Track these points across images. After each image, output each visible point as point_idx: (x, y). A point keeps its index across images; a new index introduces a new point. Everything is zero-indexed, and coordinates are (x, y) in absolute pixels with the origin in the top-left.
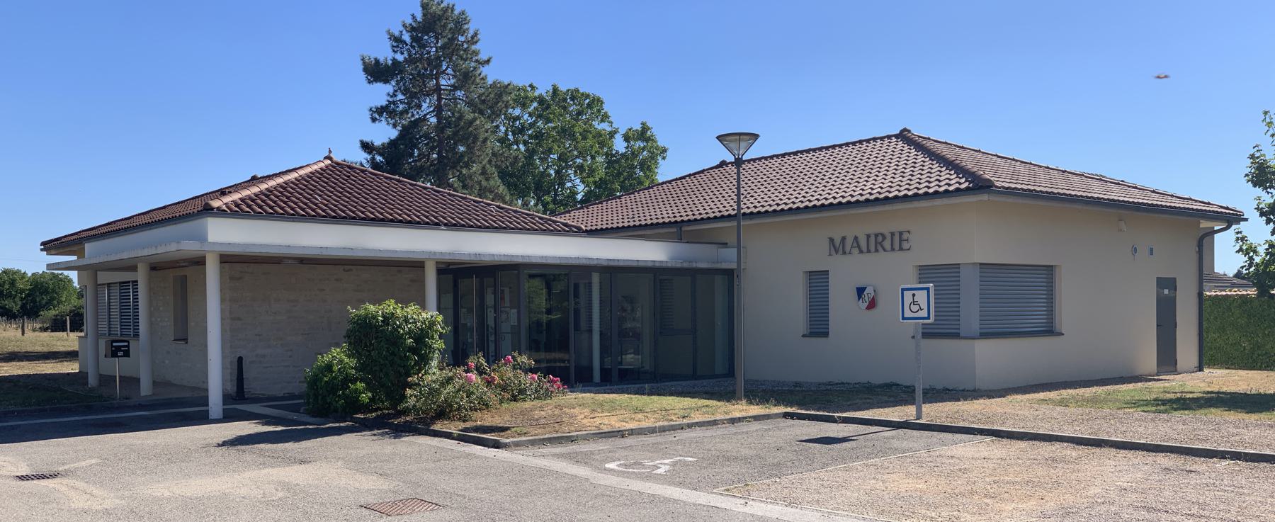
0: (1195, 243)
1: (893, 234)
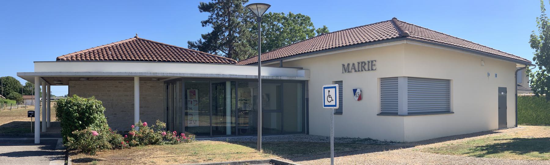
1: (369, 62)
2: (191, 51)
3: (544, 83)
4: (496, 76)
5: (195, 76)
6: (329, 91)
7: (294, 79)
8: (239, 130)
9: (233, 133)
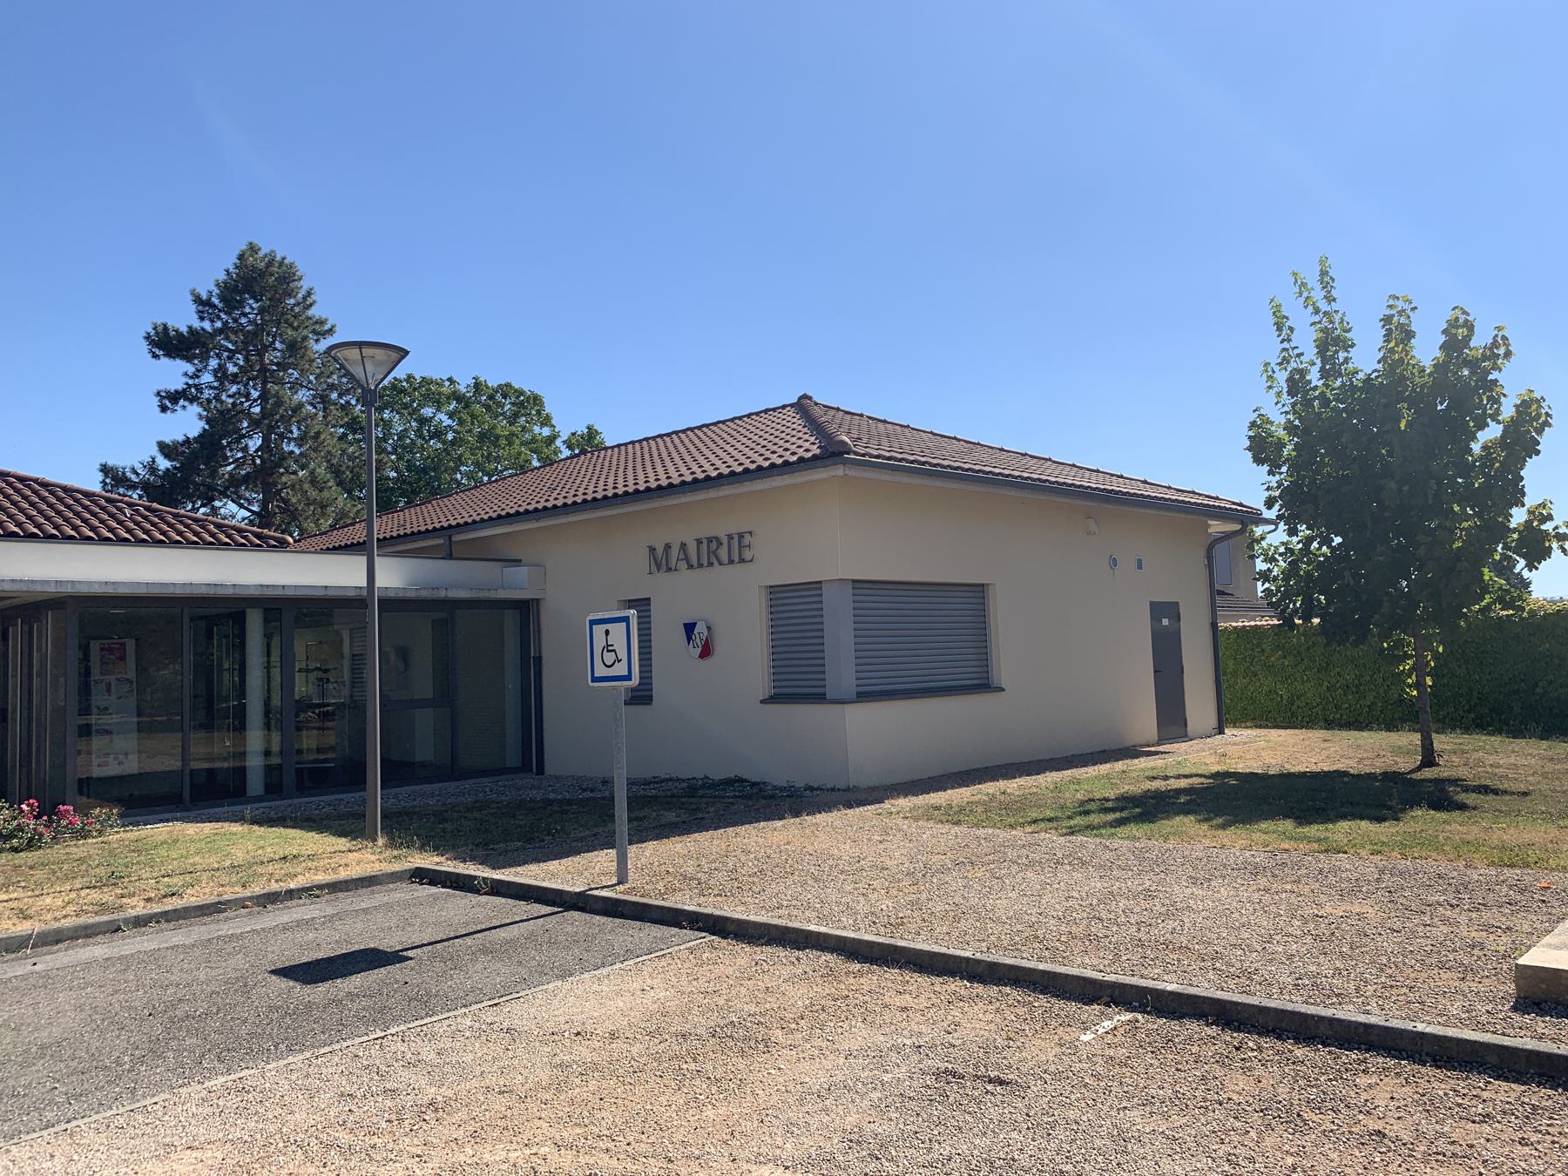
0: (1202, 553)
1: (730, 537)
2: (108, 500)
3: (1302, 580)
4: (1140, 567)
5: (122, 591)
6: (607, 632)
7: (492, 595)
8: (299, 772)
9: (274, 788)
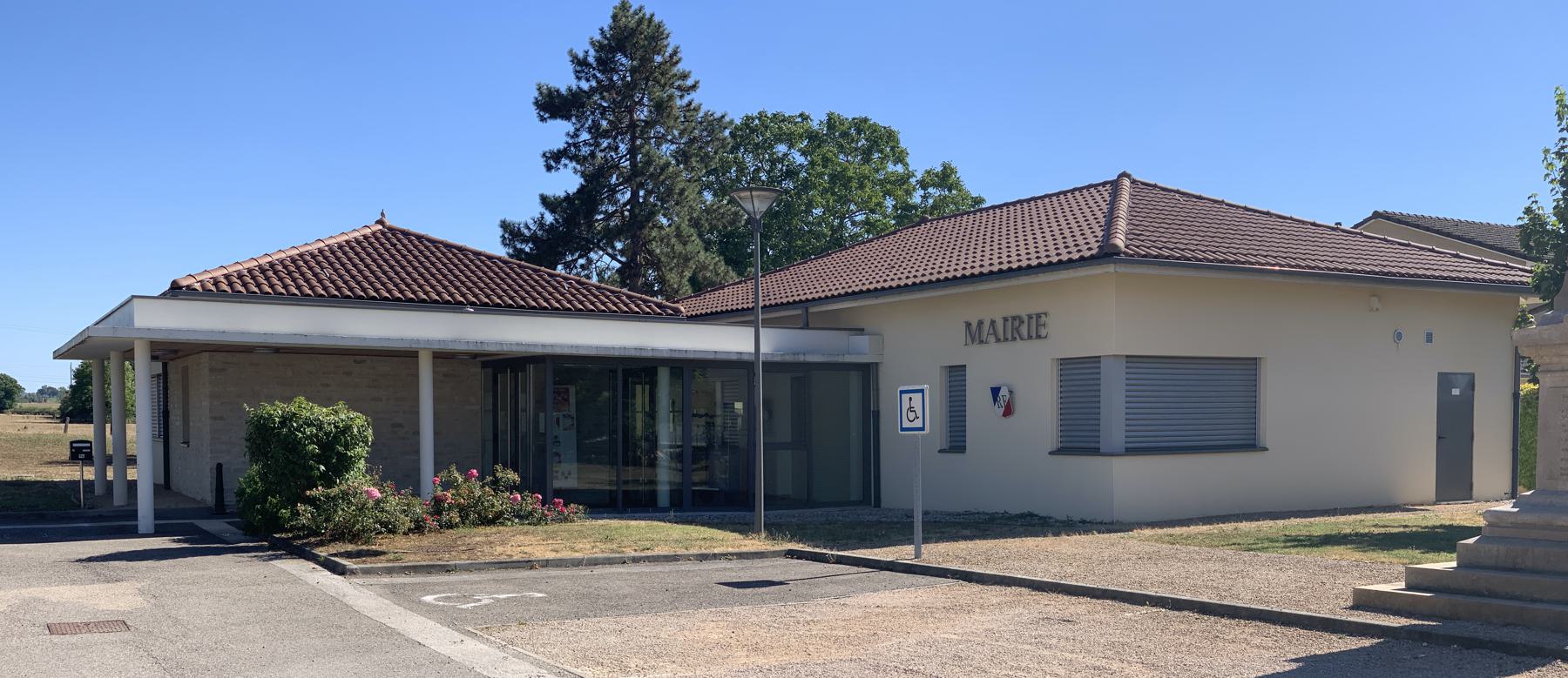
1: (1030, 317)
7: (840, 359)
